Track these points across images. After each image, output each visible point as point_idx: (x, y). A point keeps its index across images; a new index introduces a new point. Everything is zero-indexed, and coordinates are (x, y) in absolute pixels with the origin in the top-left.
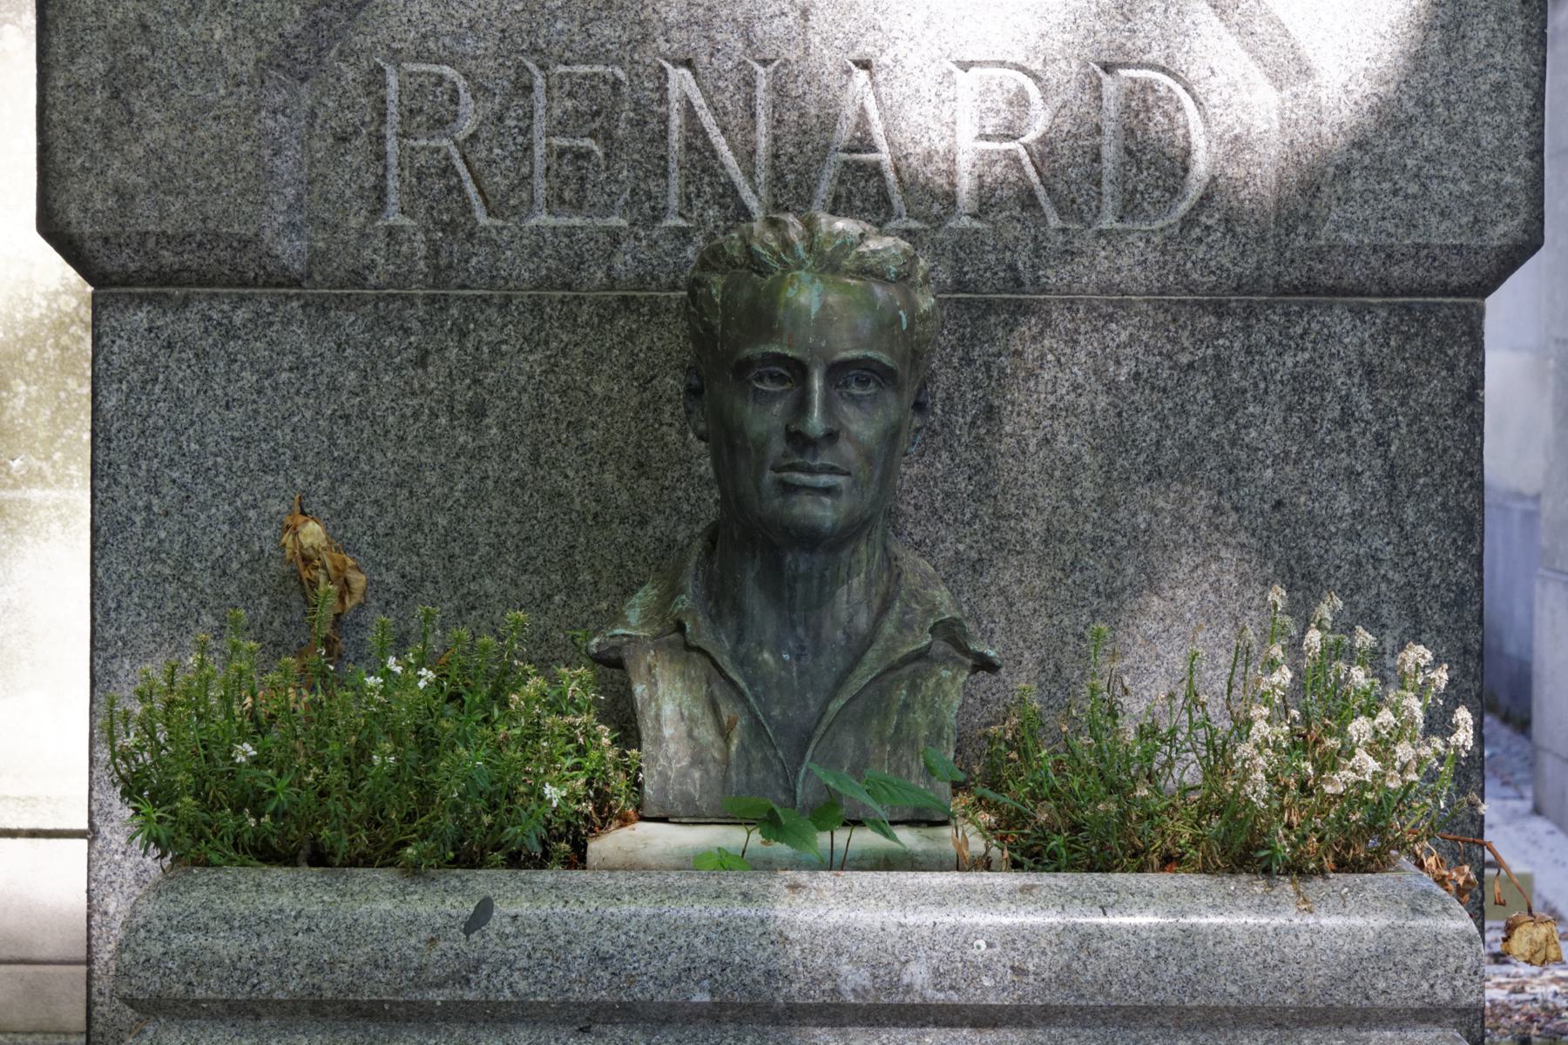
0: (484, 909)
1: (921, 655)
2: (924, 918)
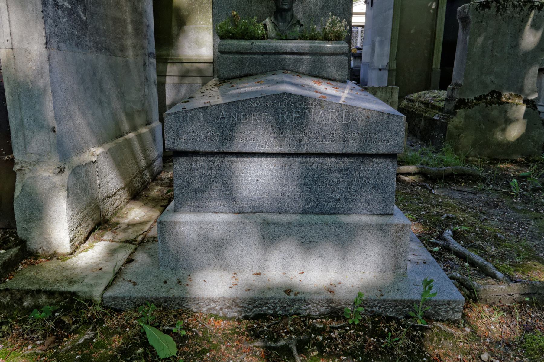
0: (253, 43)
1: (295, 23)
2: (295, 45)
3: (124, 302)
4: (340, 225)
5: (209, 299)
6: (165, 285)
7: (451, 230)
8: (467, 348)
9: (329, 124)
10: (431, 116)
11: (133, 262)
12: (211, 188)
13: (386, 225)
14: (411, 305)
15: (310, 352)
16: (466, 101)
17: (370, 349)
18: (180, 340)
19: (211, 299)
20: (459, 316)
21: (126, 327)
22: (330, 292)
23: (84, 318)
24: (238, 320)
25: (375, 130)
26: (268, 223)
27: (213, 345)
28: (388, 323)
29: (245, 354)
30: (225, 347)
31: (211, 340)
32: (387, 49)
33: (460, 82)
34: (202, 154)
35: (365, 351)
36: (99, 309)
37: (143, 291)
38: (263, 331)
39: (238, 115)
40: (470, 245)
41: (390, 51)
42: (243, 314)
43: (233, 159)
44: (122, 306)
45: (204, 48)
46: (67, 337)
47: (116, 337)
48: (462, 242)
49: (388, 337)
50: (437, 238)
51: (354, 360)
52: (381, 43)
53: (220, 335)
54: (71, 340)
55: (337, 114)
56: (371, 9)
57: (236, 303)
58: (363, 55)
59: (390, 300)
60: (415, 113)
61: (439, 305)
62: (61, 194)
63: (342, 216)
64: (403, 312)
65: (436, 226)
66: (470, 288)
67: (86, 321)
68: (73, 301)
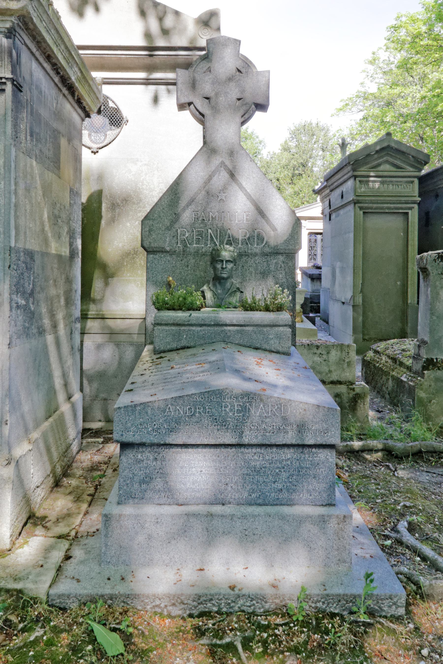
0: (191, 315)
1: (235, 291)
2: (235, 316)
3: (69, 600)
4: (283, 518)
5: (154, 595)
6: (109, 581)
7: (407, 521)
8: (409, 642)
9: (268, 417)
10: (399, 376)
11: (71, 559)
12: (155, 479)
13: (328, 516)
14: (354, 600)
15: (254, 649)
16: (435, 360)
17: (313, 645)
18: (127, 638)
19: (157, 596)
20: (402, 611)
21: (73, 625)
22: (274, 587)
23: (31, 617)
24: (183, 618)
25: (312, 421)
26: (212, 515)
27: (159, 643)
28: (332, 619)
29: (191, 652)
30: (170, 645)
31: (157, 639)
32: (350, 279)
33: (426, 339)
34: (148, 446)
35: (309, 647)
36: (46, 607)
37: (86, 589)
38: (209, 629)
39: (183, 409)
40: (426, 539)
41: (354, 283)
42: (188, 612)
43: (178, 450)
44: (67, 604)
45: (131, 302)
46: (16, 635)
47: (64, 635)
48: (417, 535)
49: (331, 633)
50: (391, 530)
51: (298, 656)
52: (343, 270)
53: (165, 633)
54: (21, 638)
55: (276, 407)
56: (330, 223)
57: (181, 599)
58: (323, 277)
59: (333, 595)
60: (381, 369)
61: (382, 600)
62: (7, 486)
63: (284, 506)
64: (346, 608)
65: (391, 516)
66: (417, 584)
67: (33, 619)
68: (19, 599)
